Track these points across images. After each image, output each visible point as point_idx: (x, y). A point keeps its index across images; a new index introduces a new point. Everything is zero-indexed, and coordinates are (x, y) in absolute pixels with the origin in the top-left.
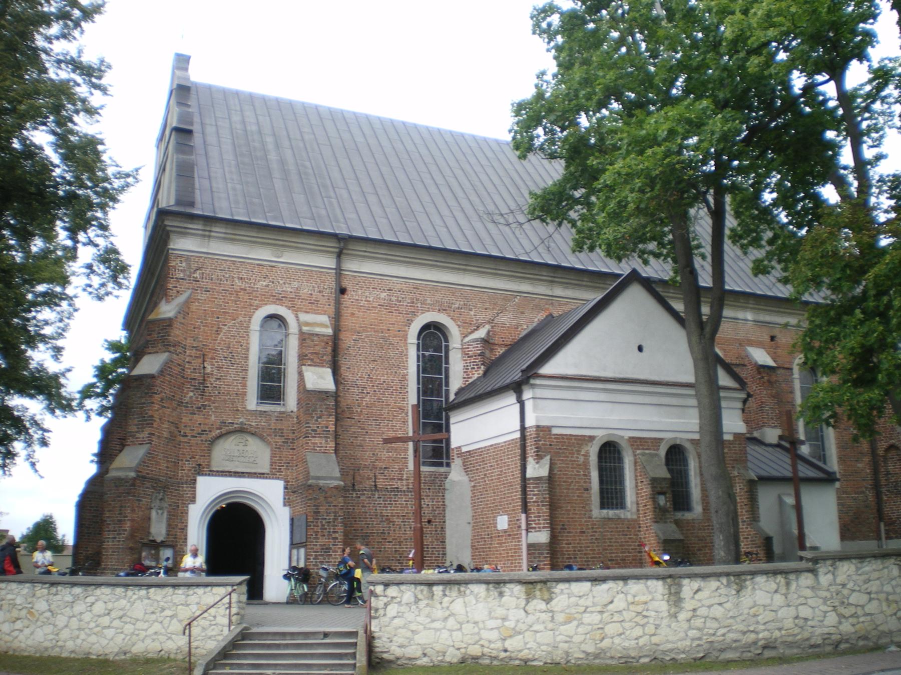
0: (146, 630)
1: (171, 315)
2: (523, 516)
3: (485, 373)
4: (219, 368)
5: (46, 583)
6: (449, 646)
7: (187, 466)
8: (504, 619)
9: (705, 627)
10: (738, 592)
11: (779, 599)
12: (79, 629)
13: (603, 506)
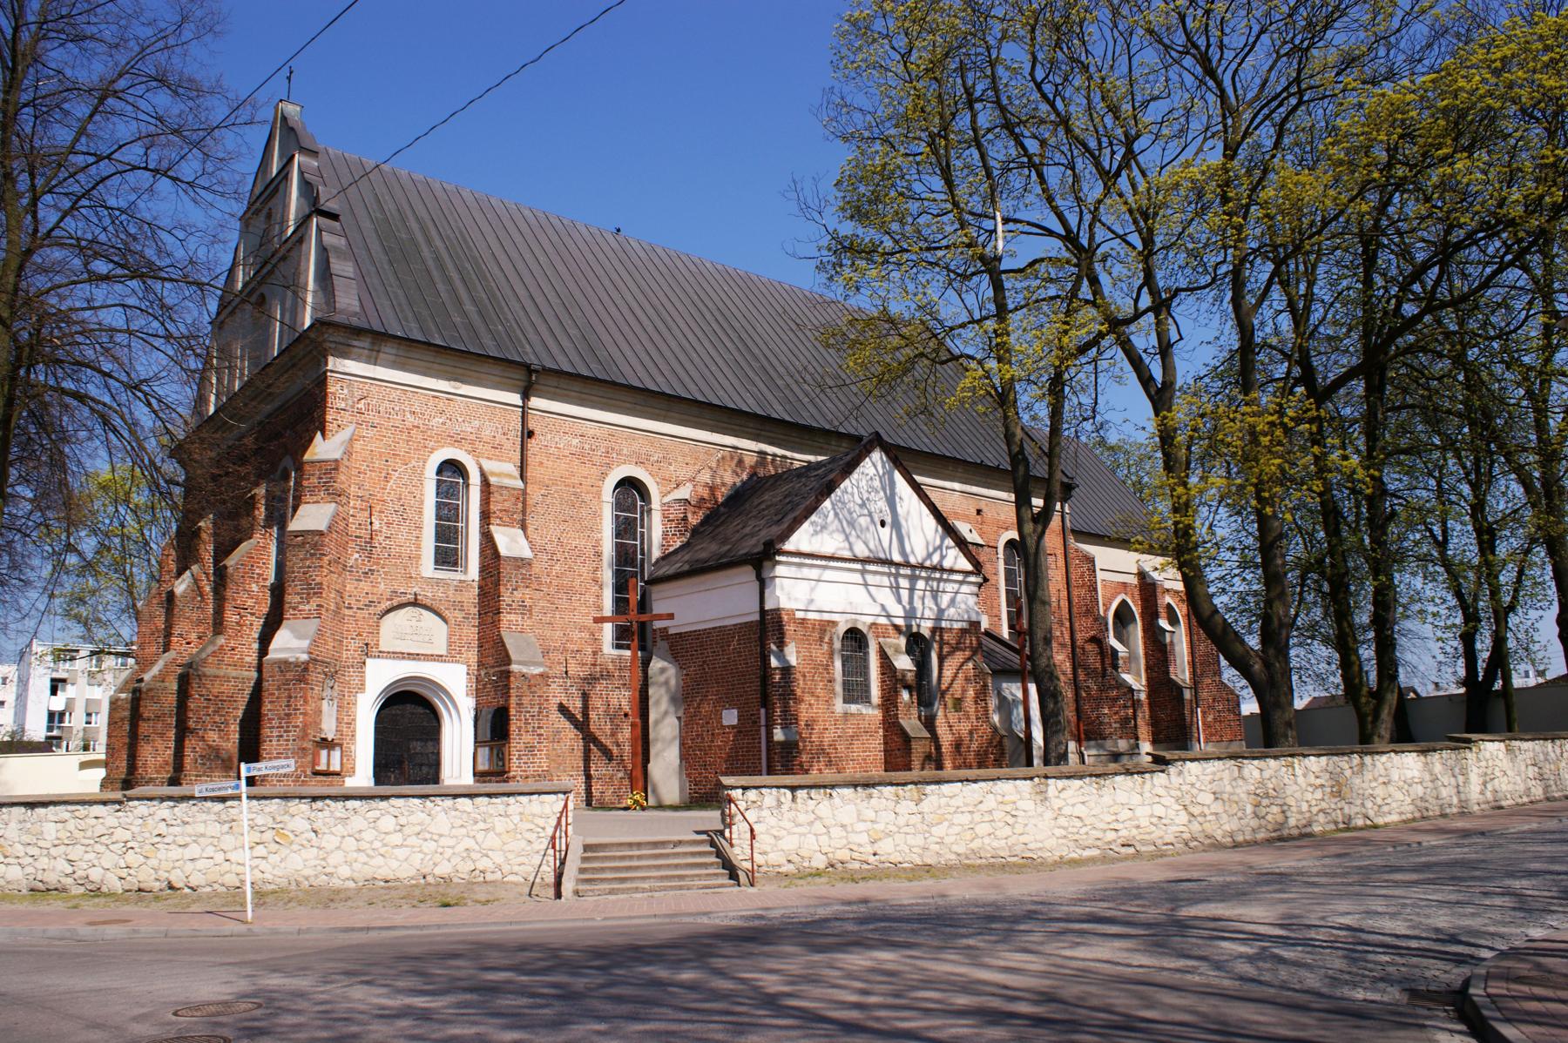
0: (453, 847)
1: (337, 455)
4: (388, 524)
7: (352, 647)
11: (1136, 799)
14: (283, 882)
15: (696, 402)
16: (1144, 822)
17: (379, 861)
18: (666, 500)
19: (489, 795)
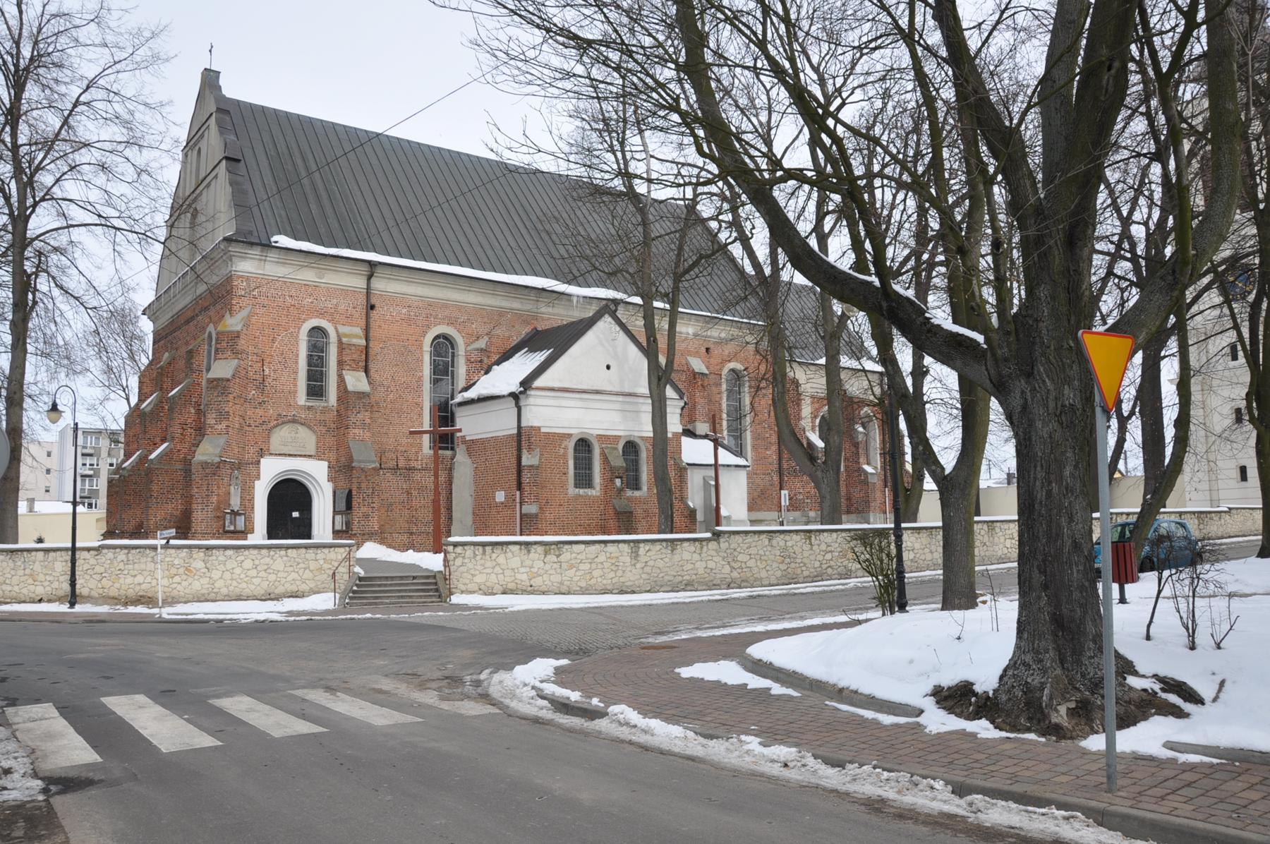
1: (239, 328)
2: (518, 493)
8: (531, 567)
11: (696, 557)
12: (232, 579)
13: (576, 486)
16: (701, 571)
17: (244, 585)
18: (469, 348)
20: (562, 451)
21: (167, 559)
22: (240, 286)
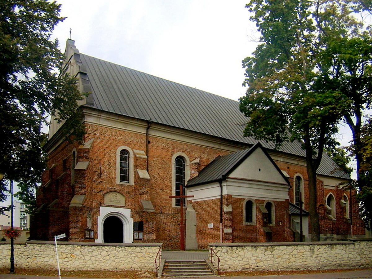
0: (125, 261)
1: (89, 147)
3: (198, 176)
4: (105, 168)
5: (79, 245)
6: (238, 265)
7: (95, 204)
9: (321, 260)
10: (331, 249)
12: (96, 261)
13: (246, 222)
14: (74, 269)
15: (185, 129)
17: (102, 264)
18: (191, 163)
19: (135, 246)
20: (241, 206)
21: (61, 250)
22: (88, 129)
